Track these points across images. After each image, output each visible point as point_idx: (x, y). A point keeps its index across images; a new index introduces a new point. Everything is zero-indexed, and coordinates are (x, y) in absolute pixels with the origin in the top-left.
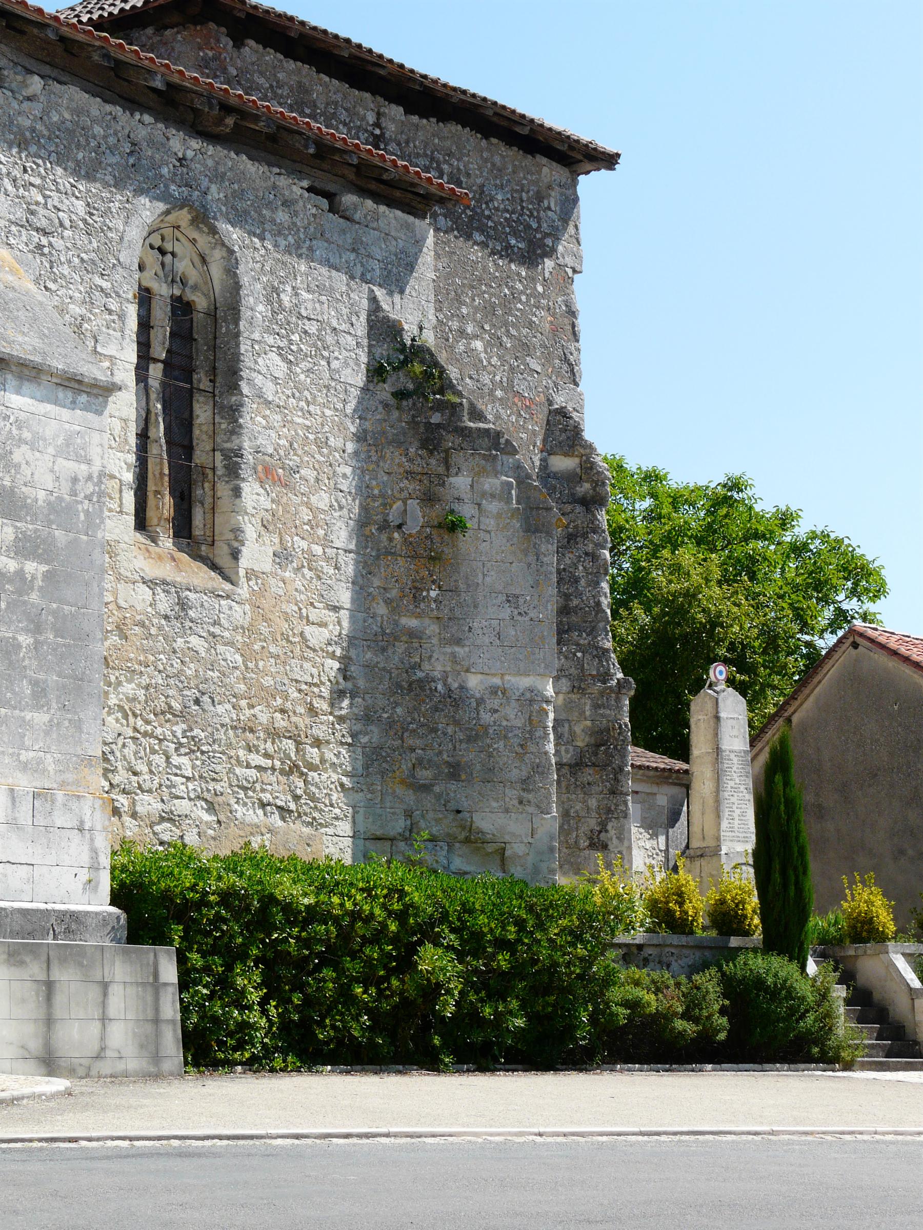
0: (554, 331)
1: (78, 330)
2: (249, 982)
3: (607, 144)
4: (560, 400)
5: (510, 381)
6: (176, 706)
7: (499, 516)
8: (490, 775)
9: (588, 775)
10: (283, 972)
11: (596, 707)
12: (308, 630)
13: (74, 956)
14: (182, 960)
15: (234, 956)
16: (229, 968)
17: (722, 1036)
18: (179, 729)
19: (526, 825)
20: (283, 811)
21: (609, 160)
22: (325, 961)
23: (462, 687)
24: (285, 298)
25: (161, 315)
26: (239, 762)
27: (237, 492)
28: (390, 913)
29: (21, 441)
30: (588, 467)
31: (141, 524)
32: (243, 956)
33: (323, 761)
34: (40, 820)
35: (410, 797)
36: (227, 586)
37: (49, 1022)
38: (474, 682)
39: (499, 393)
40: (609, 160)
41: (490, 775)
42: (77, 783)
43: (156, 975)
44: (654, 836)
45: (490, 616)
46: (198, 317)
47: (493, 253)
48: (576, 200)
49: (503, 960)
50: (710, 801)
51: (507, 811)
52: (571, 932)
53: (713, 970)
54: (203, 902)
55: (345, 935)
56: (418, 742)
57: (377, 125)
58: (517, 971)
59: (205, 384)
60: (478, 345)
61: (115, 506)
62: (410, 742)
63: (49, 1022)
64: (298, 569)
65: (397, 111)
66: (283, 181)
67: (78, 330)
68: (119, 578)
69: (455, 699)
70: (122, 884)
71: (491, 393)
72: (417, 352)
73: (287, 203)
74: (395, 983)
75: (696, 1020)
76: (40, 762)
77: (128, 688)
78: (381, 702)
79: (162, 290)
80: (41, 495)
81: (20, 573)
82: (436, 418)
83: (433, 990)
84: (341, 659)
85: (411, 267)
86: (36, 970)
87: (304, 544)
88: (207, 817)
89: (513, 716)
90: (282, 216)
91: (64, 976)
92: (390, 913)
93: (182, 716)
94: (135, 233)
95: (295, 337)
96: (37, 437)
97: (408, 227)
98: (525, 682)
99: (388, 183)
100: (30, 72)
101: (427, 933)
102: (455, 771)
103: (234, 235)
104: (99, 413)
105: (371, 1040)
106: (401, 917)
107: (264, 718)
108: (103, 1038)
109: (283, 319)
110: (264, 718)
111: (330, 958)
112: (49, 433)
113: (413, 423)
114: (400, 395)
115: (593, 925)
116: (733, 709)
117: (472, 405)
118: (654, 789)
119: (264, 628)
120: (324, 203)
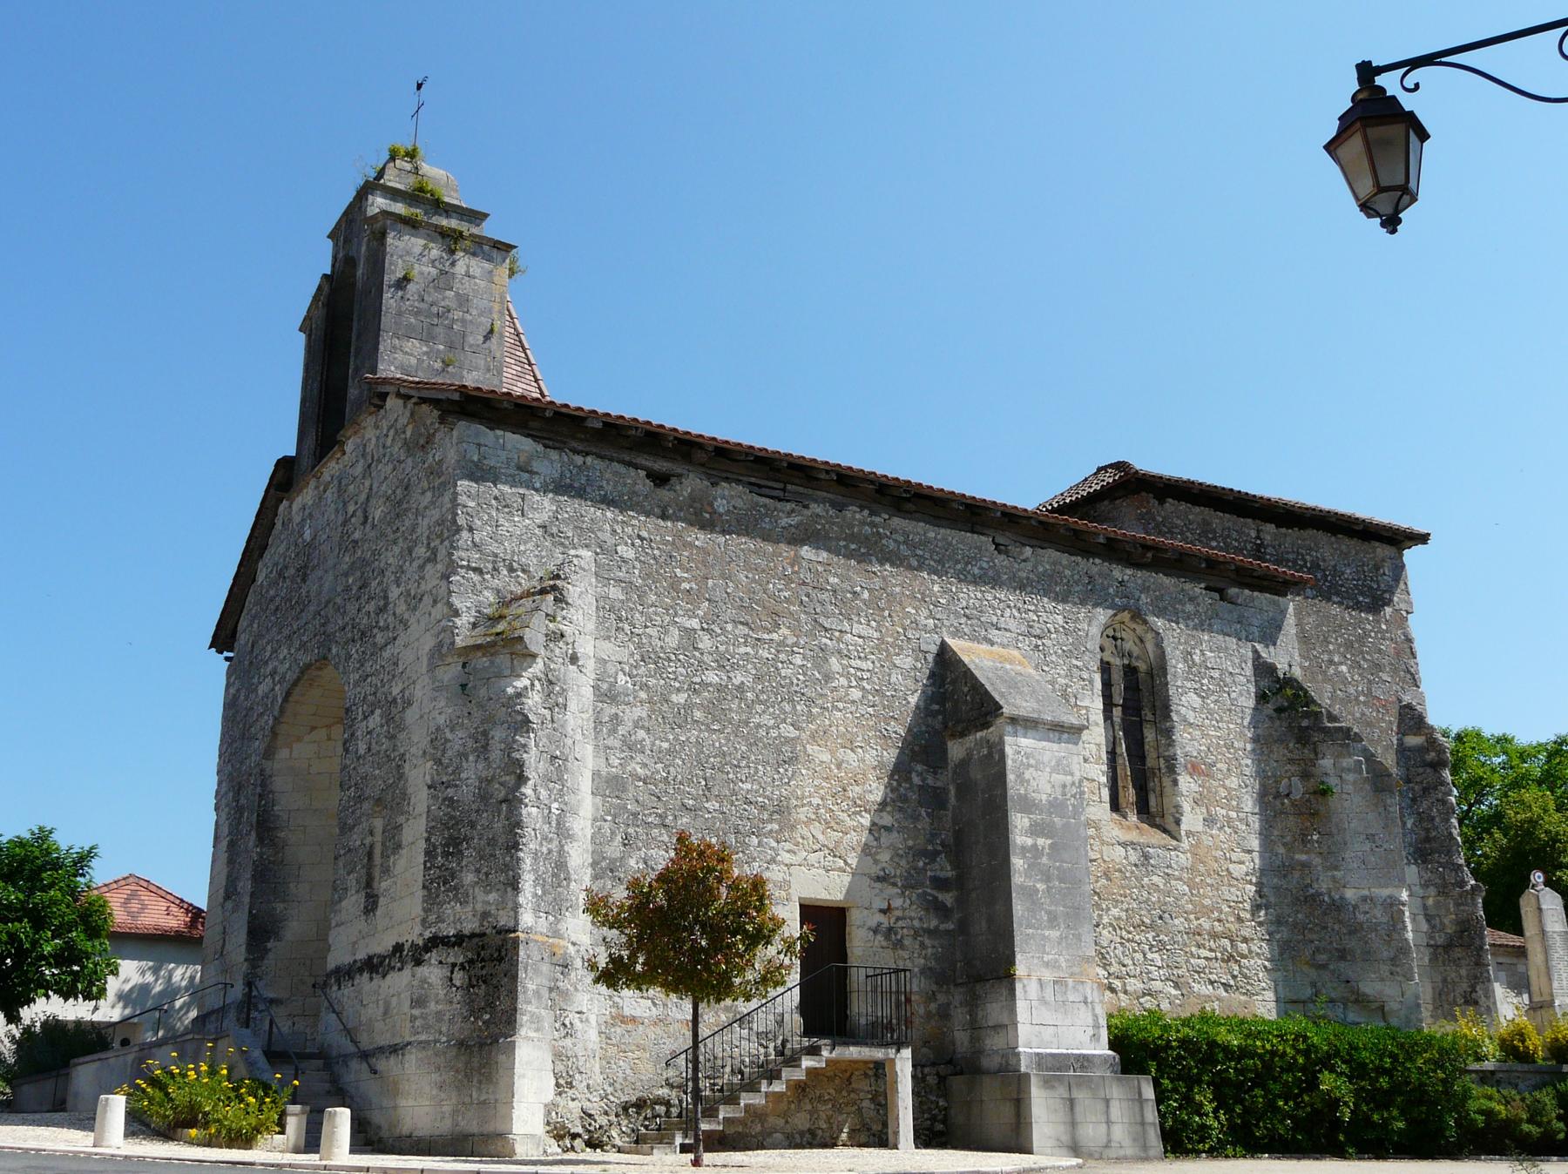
0: (1398, 654)
1: (1065, 696)
2: (1204, 1098)
3: (1420, 528)
4: (1407, 699)
5: (1369, 690)
6: (1147, 921)
7: (1355, 783)
8: (1368, 956)
9: (1458, 953)
10: (1226, 1090)
11: (1457, 905)
12: (1231, 866)
13: (1083, 1082)
14: (1157, 1084)
15: (1193, 1082)
16: (1190, 1089)
17: (1561, 1136)
18: (1150, 936)
19: (1410, 991)
20: (1226, 986)
21: (1423, 538)
22: (1255, 1085)
23: (1342, 898)
24: (1196, 658)
25: (1117, 676)
26: (1193, 956)
27: (1175, 782)
28: (1298, 1051)
29: (1029, 766)
30: (1432, 743)
31: (1115, 806)
32: (1199, 1082)
33: (1250, 951)
34: (1059, 998)
35: (1313, 973)
36: (1174, 843)
37: (1073, 1124)
38: (1350, 894)
39: (1362, 698)
40: (1423, 538)
41: (1368, 956)
42: (1081, 974)
43: (1140, 1094)
44: (1519, 994)
45: (1357, 849)
46: (1141, 676)
47: (1347, 607)
48: (1403, 566)
49: (1384, 1082)
50: (1543, 968)
51: (1382, 980)
52: (1435, 1063)
53: (1550, 1089)
54: (1168, 1045)
55: (1268, 1066)
56: (1315, 936)
57: (1258, 537)
58: (1395, 1089)
59: (1150, 717)
60: (1344, 668)
61: (1096, 798)
62: (1309, 936)
63: (1073, 1124)
64: (1221, 828)
65: (1271, 527)
66: (1188, 586)
67: (1065, 696)
68: (1103, 843)
69: (1338, 906)
70: (1116, 1037)
71: (1357, 698)
72: (1289, 682)
73: (1192, 599)
74: (1306, 1098)
75: (1539, 1125)
76: (1056, 961)
77: (1115, 912)
78: (1287, 910)
79: (1117, 662)
80: (1044, 797)
81: (1035, 846)
82: (1305, 723)
83: (1334, 1103)
84: (1256, 885)
85: (1279, 628)
86: (1062, 1091)
87: (1224, 812)
88: (1174, 992)
89: (1379, 915)
90: (1189, 608)
91: (1079, 1094)
92: (1298, 1051)
93: (1152, 927)
94: (1095, 631)
95: (1205, 681)
96: (1038, 762)
97: (1276, 604)
98: (1385, 892)
99: (1258, 577)
100: (1024, 545)
101: (1326, 1063)
102: (1343, 955)
103: (1159, 623)
104: (1076, 744)
105: (1294, 1136)
106: (1306, 1054)
107: (1207, 926)
108: (1108, 1135)
109: (1196, 671)
110: (1207, 926)
111: (1259, 1081)
112: (1046, 759)
113: (1290, 727)
114: (1279, 710)
115: (1449, 1056)
116: (1551, 901)
117: (1329, 713)
118: (1515, 961)
119: (1202, 868)
120: (1217, 596)
